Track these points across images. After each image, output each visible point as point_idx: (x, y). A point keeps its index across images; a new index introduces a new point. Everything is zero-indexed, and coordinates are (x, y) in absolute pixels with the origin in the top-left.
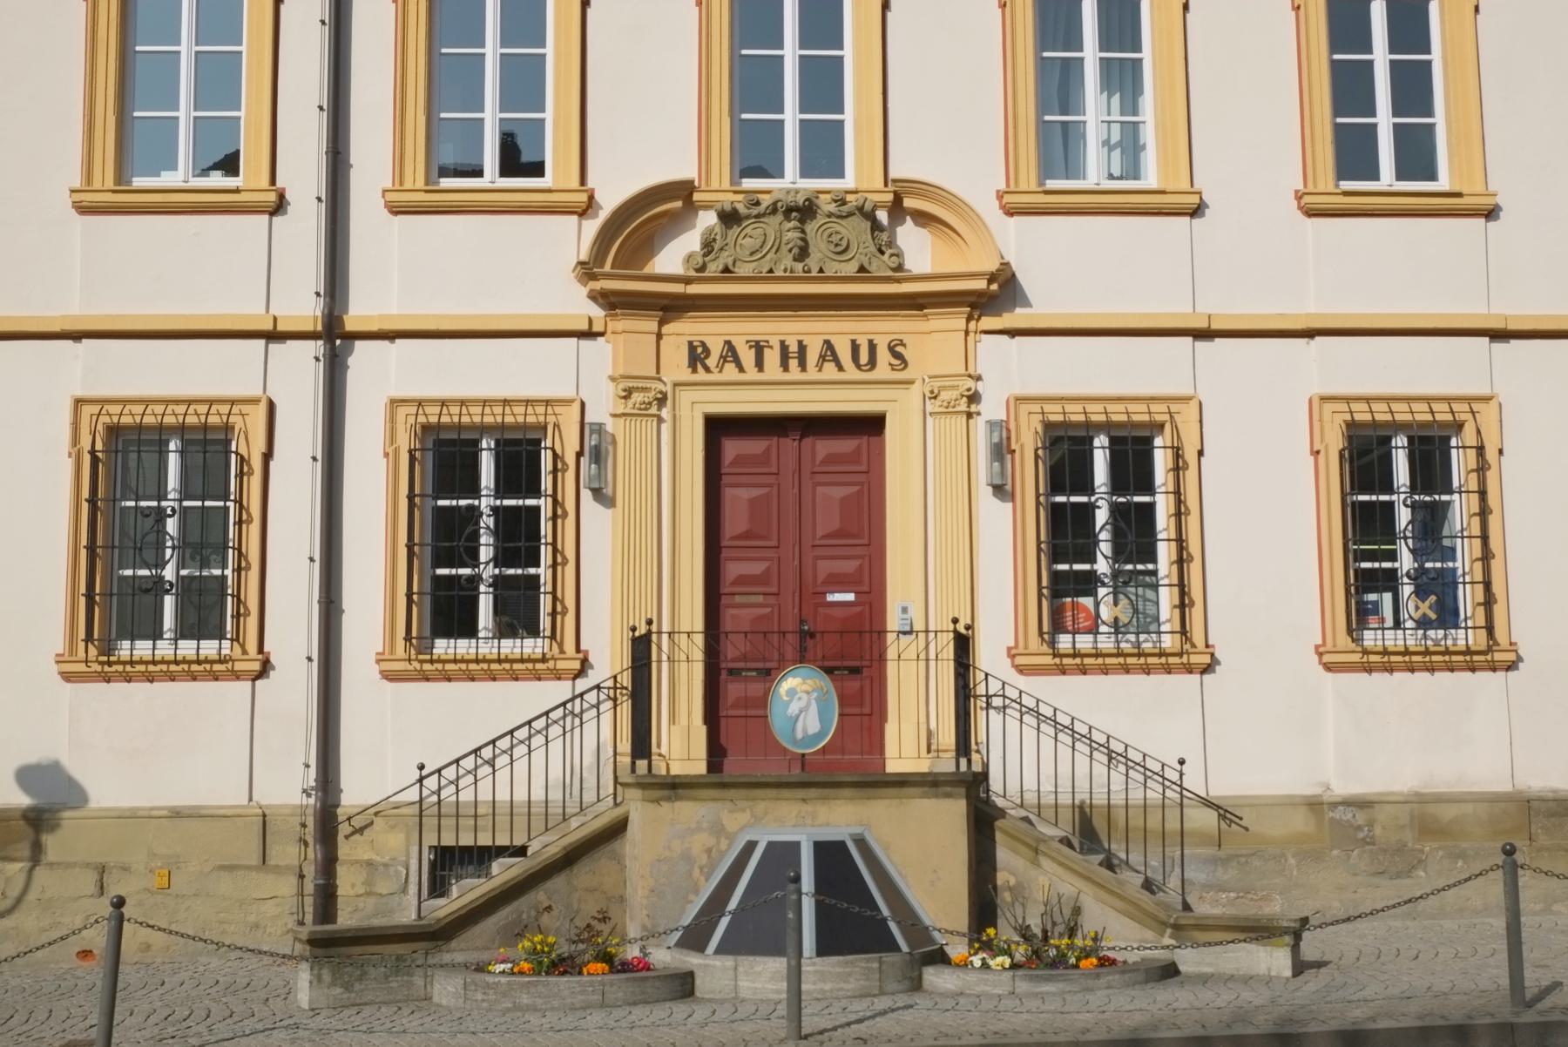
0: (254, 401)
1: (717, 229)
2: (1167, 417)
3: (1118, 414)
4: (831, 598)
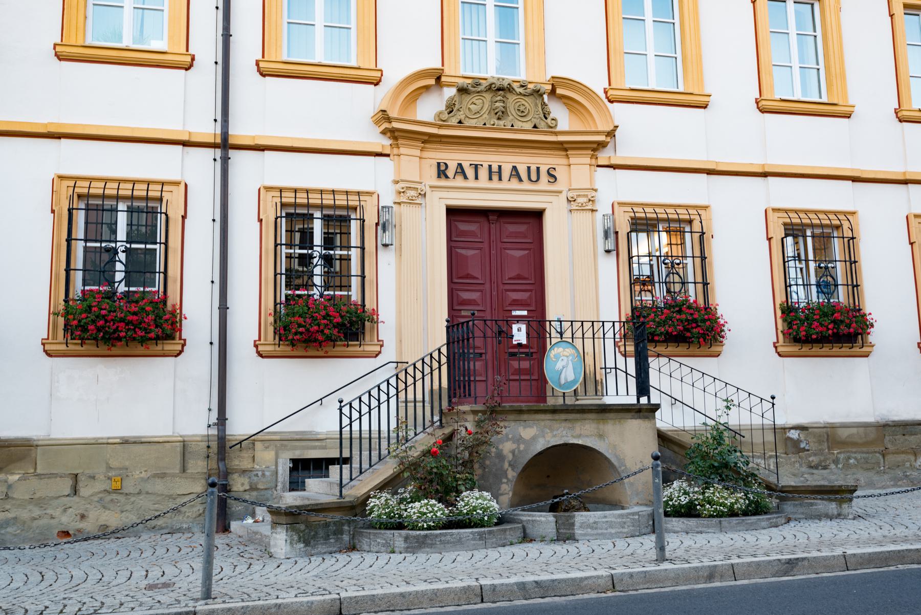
0: (177, 183)
1: (457, 99)
2: (358, 203)
3: (328, 200)
4: (514, 313)
